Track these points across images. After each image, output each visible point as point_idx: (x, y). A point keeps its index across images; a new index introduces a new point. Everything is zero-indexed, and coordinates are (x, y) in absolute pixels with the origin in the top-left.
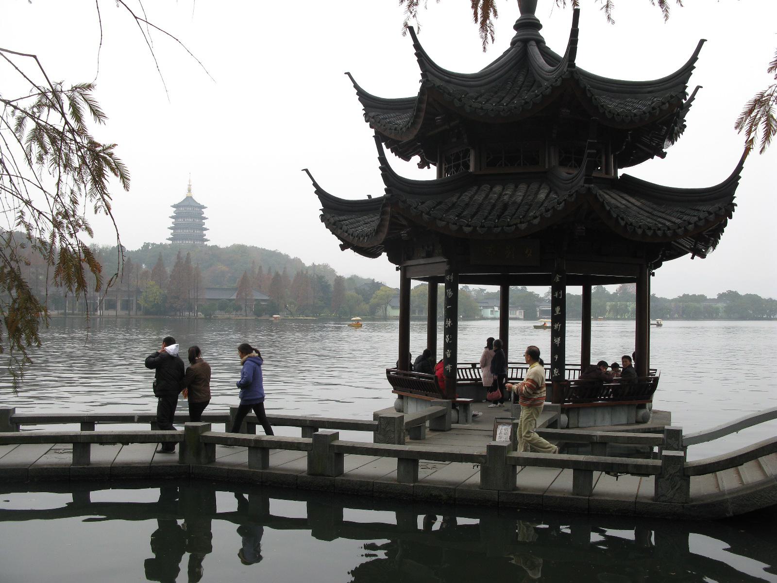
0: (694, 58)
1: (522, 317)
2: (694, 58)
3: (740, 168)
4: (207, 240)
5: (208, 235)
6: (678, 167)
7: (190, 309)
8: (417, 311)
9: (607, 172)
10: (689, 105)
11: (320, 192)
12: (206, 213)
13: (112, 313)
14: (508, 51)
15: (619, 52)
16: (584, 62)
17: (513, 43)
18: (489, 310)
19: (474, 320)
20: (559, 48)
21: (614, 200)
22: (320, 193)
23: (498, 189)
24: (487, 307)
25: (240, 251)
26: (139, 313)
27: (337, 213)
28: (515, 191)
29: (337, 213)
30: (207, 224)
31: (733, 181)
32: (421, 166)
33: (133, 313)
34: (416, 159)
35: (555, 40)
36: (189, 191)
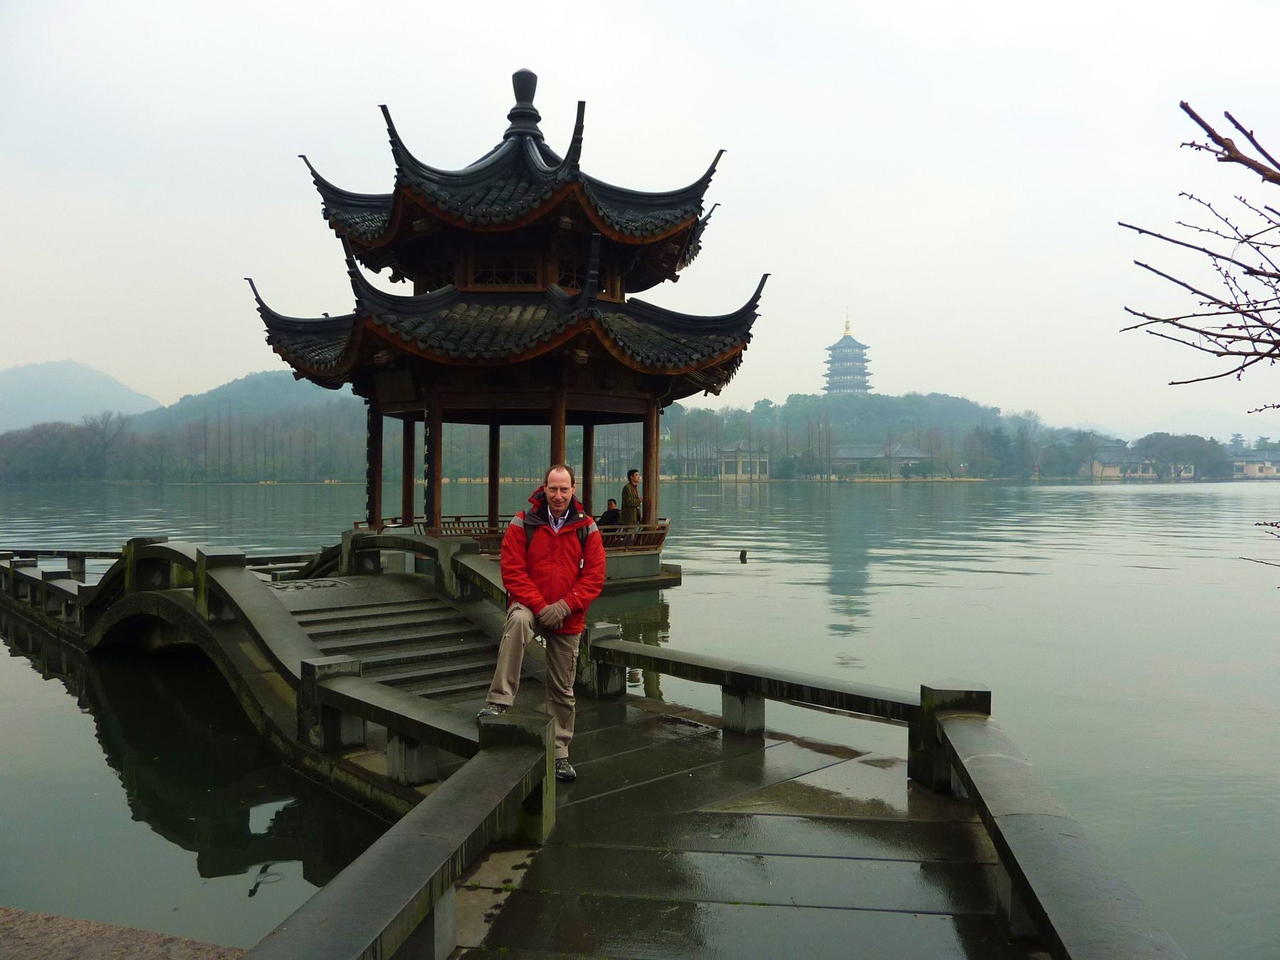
0: (712, 170)
2: (712, 170)
3: (757, 296)
5: (871, 381)
6: (689, 293)
7: (820, 471)
8: (1140, 468)
10: (704, 223)
12: (868, 354)
13: (732, 477)
14: (500, 146)
15: (627, 159)
16: (590, 166)
17: (506, 137)
18: (1257, 466)
19: (1231, 480)
20: (560, 148)
22: (321, 184)
23: (531, 310)
24: (1253, 463)
26: (762, 477)
27: (282, 332)
28: (524, 310)
29: (282, 332)
30: (870, 367)
32: (393, 279)
33: (755, 477)
34: (387, 271)
36: (847, 328)
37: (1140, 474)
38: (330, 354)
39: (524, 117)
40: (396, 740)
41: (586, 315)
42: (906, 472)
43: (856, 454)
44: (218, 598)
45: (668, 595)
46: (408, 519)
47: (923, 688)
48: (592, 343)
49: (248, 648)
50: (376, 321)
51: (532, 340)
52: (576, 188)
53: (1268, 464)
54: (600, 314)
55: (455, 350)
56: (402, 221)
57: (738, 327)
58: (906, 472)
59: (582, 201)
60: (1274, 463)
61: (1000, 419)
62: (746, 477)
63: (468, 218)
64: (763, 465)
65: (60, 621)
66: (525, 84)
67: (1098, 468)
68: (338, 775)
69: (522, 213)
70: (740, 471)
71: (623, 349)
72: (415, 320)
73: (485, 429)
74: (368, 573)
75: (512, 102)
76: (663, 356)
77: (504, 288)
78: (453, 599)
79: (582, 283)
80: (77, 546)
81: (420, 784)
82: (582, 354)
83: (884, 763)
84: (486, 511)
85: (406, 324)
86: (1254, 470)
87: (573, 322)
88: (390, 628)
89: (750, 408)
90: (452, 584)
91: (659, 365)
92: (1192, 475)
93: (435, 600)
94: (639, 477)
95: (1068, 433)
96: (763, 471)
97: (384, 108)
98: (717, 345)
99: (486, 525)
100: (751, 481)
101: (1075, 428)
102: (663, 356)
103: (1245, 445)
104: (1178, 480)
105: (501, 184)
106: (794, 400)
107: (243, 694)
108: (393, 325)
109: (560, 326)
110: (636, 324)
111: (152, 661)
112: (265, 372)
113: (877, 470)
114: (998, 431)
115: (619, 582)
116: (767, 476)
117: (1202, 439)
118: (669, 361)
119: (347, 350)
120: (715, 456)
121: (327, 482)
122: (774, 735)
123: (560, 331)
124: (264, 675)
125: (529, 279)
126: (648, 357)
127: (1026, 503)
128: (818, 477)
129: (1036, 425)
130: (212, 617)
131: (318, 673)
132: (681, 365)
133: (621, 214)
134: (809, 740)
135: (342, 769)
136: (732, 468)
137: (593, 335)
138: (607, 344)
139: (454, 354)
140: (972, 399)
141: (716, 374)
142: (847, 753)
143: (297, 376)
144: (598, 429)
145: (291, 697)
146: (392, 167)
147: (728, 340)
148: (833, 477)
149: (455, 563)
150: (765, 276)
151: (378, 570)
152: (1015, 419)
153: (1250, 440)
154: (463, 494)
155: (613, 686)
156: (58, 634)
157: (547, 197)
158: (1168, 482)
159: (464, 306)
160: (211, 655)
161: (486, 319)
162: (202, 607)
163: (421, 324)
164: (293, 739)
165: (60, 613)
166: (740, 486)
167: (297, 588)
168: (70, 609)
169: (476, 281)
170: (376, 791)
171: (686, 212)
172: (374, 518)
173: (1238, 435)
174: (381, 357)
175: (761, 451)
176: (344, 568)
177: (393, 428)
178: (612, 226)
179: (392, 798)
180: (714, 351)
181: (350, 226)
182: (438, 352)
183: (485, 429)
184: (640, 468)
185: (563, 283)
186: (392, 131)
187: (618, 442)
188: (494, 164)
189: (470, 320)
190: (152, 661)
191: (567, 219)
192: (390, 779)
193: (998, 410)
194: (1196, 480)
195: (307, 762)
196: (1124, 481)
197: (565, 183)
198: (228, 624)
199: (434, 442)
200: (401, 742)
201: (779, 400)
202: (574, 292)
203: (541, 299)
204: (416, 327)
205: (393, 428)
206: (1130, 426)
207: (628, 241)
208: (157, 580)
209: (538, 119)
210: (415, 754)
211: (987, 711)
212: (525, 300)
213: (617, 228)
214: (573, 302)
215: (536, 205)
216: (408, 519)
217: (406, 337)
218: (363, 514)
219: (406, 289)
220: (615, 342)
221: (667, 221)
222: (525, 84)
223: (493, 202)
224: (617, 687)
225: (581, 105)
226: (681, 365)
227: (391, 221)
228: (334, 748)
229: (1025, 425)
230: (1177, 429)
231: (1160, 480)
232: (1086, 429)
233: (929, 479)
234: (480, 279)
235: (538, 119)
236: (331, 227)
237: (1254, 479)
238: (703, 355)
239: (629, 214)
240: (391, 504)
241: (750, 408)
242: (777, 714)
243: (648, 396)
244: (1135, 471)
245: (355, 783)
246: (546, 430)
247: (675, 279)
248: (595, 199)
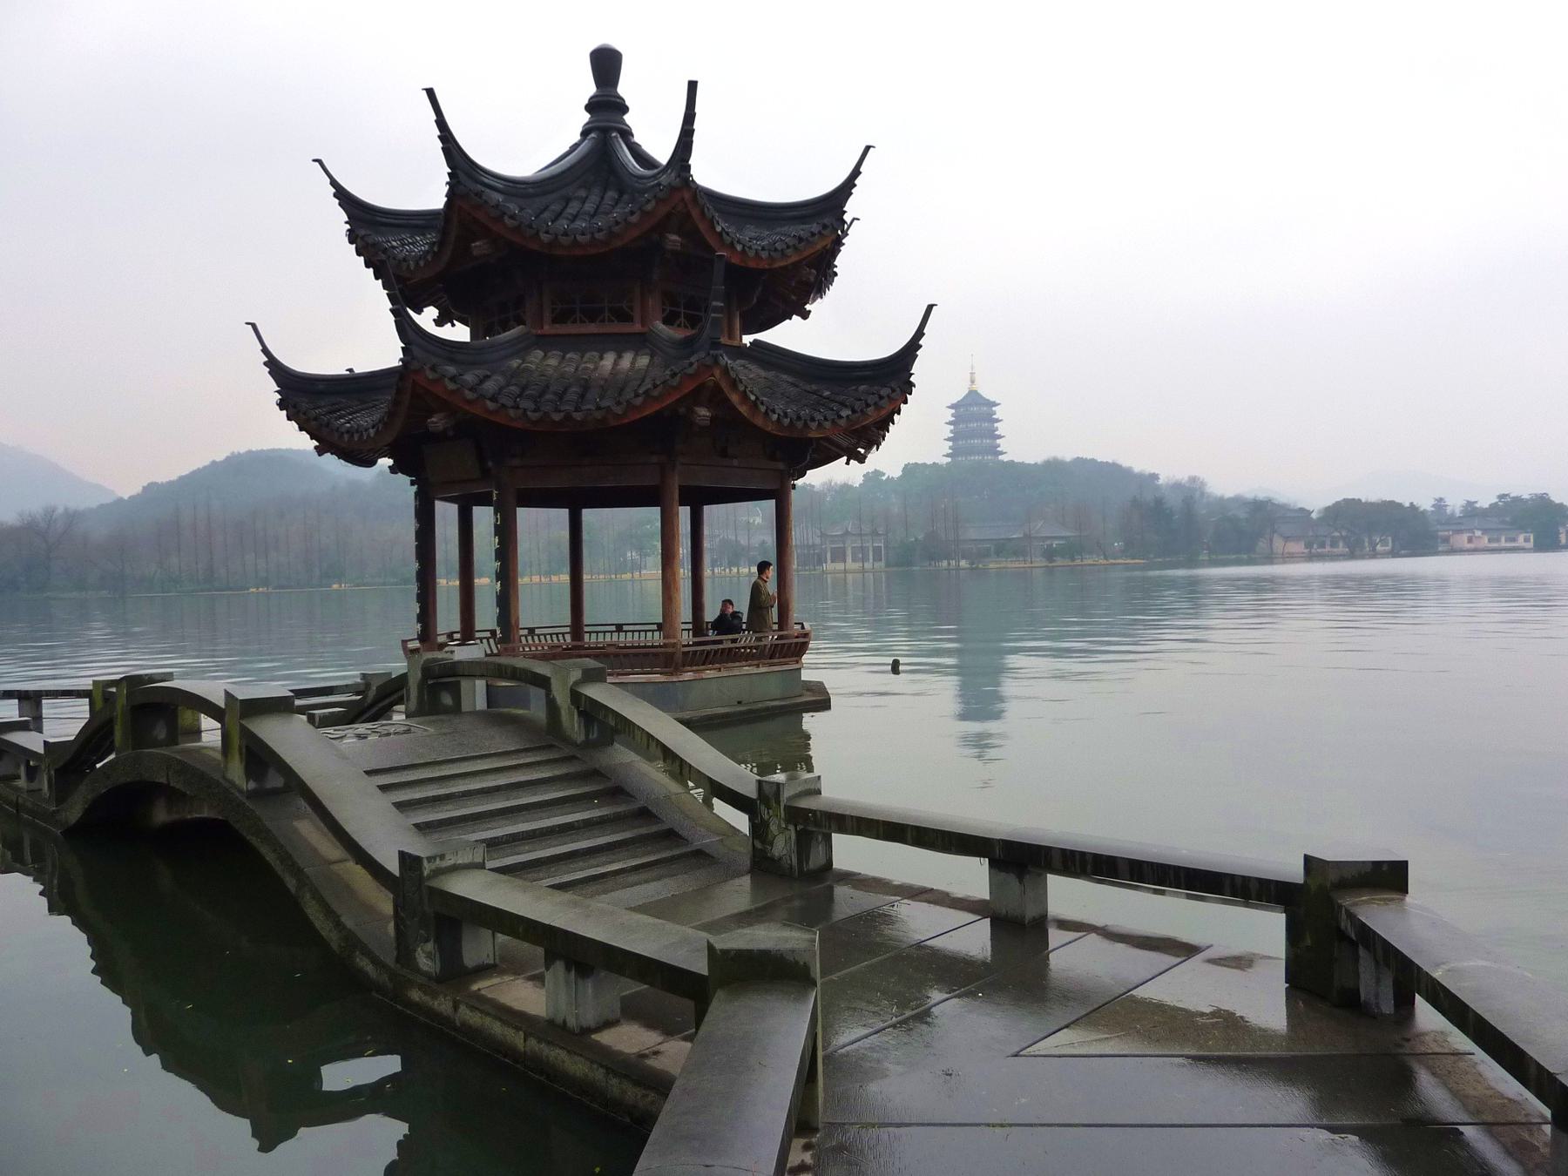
0: (856, 173)
1: (1531, 545)
2: (856, 173)
5: (1003, 444)
6: (822, 332)
7: (948, 557)
8: (1328, 542)
9: (731, 336)
12: (999, 412)
13: (840, 566)
14: (574, 147)
16: (706, 172)
17: (585, 134)
18: (1465, 536)
21: (750, 374)
22: (345, 198)
24: (1460, 532)
25: (1053, 468)
26: (877, 565)
27: (302, 395)
28: (620, 357)
29: (302, 395)
30: (1001, 428)
31: (910, 351)
32: (439, 322)
33: (868, 566)
34: (431, 312)
35: (655, 136)
37: (1328, 549)
38: (366, 420)
39: (607, 108)
40: (559, 966)
41: (709, 361)
42: (1050, 554)
44: (260, 758)
45: (810, 722)
46: (468, 633)
47: (1307, 859)
48: (716, 398)
49: (309, 830)
50: (431, 375)
51: (637, 396)
52: (687, 196)
53: (1478, 533)
54: (726, 360)
55: (535, 411)
56: (456, 247)
57: (890, 379)
58: (1050, 554)
59: (695, 213)
60: (1485, 531)
61: (1158, 488)
62: (857, 566)
63: (545, 237)
64: (877, 551)
65: (17, 789)
66: (606, 64)
67: (1278, 544)
68: (466, 1015)
69: (616, 229)
70: (849, 559)
71: (754, 405)
72: (480, 372)
73: (563, 514)
74: (447, 711)
75: (590, 89)
76: (805, 413)
77: (592, 328)
78: (574, 744)
79: (693, 321)
80: (53, 688)
81: (598, 1029)
82: (703, 412)
83: (1240, 962)
84: (566, 618)
85: (469, 378)
86: (1462, 540)
87: (690, 371)
88: (497, 789)
90: (572, 724)
91: (800, 425)
92: (1388, 548)
93: (550, 747)
94: (772, 572)
95: (1238, 501)
96: (877, 558)
97: (430, 93)
99: (568, 638)
100: (863, 571)
101: (1250, 495)
102: (805, 413)
103: (1449, 511)
104: (1374, 555)
105: (582, 193)
107: (308, 896)
109: (674, 375)
110: (763, 373)
111: (163, 847)
112: (250, 452)
113: (1016, 553)
114: (1159, 502)
115: (754, 707)
116: (883, 564)
117: (1400, 505)
118: (813, 419)
119: (391, 414)
120: (818, 541)
121: (335, 586)
122: (1064, 925)
123: (675, 382)
124: (335, 867)
125: (625, 317)
126: (786, 415)
127: (1194, 593)
128: (945, 563)
129: (1202, 494)
130: (252, 785)
131: (427, 868)
132: (827, 425)
133: (740, 230)
134: (1115, 930)
135: (473, 1008)
136: (839, 556)
137: (717, 389)
138: (735, 398)
139: (534, 416)
140: (1125, 462)
141: (864, 435)
142: (1187, 950)
143: (320, 451)
144: (708, 510)
145: (384, 903)
146: (443, 171)
147: (885, 392)
148: (963, 563)
149: (576, 697)
152: (1177, 486)
153: (1455, 504)
154: (542, 601)
155: (816, 860)
156: (17, 806)
157: (649, 207)
158: (1363, 557)
159: (540, 353)
160: (254, 841)
162: (235, 771)
163: (487, 377)
164: (389, 959)
165: (19, 777)
166: (850, 577)
167: (359, 736)
168: (32, 773)
169: (555, 321)
170: (532, 1042)
171: (825, 227)
173: (1441, 499)
174: (437, 422)
175: (875, 533)
177: (446, 513)
179: (563, 1054)
180: (868, 405)
181: (385, 251)
182: (512, 413)
183: (563, 514)
184: (773, 558)
185: (668, 321)
186: (441, 123)
187: (741, 526)
189: (550, 371)
190: (163, 847)
191: (674, 237)
192: (551, 1022)
193: (1155, 477)
194: (1394, 554)
195: (416, 995)
196: (1311, 558)
197: (672, 189)
198: (275, 792)
199: (506, 532)
200: (568, 969)
202: (689, 332)
203: (641, 342)
204: (482, 382)
205: (446, 513)
206: (1312, 487)
207: (752, 264)
208: (161, 732)
209: (625, 109)
210: (589, 987)
211: (1403, 888)
212: (620, 343)
213: (739, 248)
214: (688, 344)
215: (634, 219)
216: (468, 633)
217: (469, 395)
219: (459, 333)
220: (744, 397)
221: (800, 239)
222: (606, 64)
223: (575, 218)
224: (822, 861)
225: (693, 86)
226: (827, 425)
228: (455, 974)
229: (1190, 493)
230: (1371, 492)
231: (1352, 556)
232: (1261, 496)
233: (1078, 562)
234: (558, 319)
235: (624, 109)
236: (359, 254)
237: (1461, 551)
238: (854, 411)
239: (749, 232)
240: (448, 618)
242: (1065, 895)
243: (781, 466)
244: (1323, 545)
245: (497, 1028)
246: (655, 512)
248: (711, 211)
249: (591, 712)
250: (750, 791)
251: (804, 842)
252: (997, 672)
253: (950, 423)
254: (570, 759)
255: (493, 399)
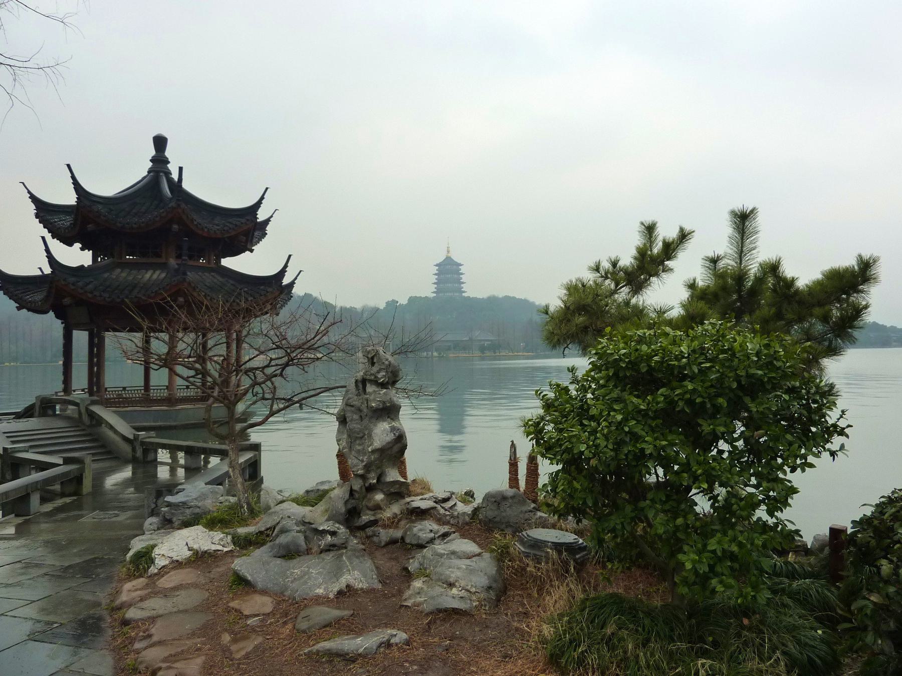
0: (262, 198)
2: (262, 198)
4: (464, 292)
5: (465, 287)
11: (34, 198)
12: (463, 269)
14: (145, 177)
15: (212, 183)
17: (149, 172)
22: (34, 199)
23: (158, 272)
25: (492, 301)
28: (154, 272)
30: (464, 278)
36: (448, 252)
38: (38, 297)
39: (160, 161)
43: (450, 337)
50: (63, 283)
58: (483, 349)
66: (160, 143)
74: (49, 416)
75: (153, 152)
84: (142, 383)
85: (80, 284)
89: (382, 306)
90: (85, 418)
97: (68, 166)
98: (273, 290)
106: (412, 300)
108: (73, 284)
110: (221, 279)
113: (464, 349)
128: (425, 354)
140: (531, 300)
149: (87, 409)
150: (290, 256)
151: (55, 415)
155: (151, 457)
159: (119, 270)
161: (131, 278)
172: (67, 389)
176: (37, 414)
178: (202, 229)
186: (73, 177)
188: (139, 190)
201: (403, 301)
203: (163, 266)
212: (154, 267)
215: (157, 219)
218: (60, 387)
221: (236, 225)
222: (160, 143)
227: (75, 220)
241: (382, 306)
247: (252, 251)
249: (92, 415)
250: (131, 437)
251: (146, 452)
252: (462, 415)
253: (436, 274)
254: (83, 430)
255: (91, 292)
